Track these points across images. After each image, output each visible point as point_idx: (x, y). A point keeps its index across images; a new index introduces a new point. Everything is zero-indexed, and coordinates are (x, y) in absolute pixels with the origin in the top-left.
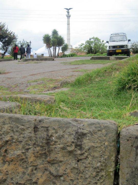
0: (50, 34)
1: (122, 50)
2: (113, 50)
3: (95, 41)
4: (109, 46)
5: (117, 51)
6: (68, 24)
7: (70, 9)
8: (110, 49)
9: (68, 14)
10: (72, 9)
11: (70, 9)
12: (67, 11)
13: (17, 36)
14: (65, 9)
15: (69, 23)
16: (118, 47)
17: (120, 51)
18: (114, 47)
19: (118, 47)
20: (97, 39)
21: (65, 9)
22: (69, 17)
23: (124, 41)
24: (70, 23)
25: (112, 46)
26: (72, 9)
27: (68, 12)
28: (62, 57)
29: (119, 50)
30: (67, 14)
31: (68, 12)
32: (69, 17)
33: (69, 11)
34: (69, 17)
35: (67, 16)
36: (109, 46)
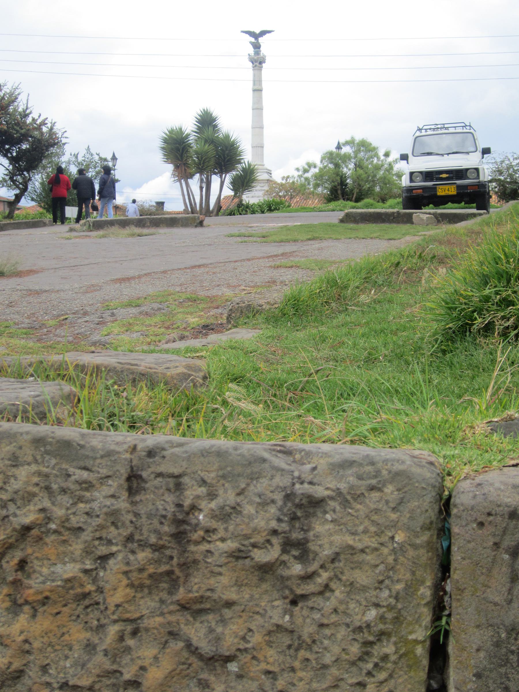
0: (189, 126)
1: (459, 187)
2: (424, 188)
3: (357, 152)
4: (412, 174)
5: (441, 192)
6: (254, 90)
7: (263, 33)
9: (257, 53)
10: (269, 32)
11: (263, 33)
12: (253, 40)
16: (444, 176)
17: (452, 191)
18: (429, 175)
20: (364, 146)
22: (258, 62)
23: (468, 153)
24: (264, 85)
25: (421, 172)
26: (269, 32)
27: (257, 46)
28: (231, 214)
29: (447, 187)
30: (251, 50)
31: (257, 46)
32: (258, 62)
33: (260, 40)
34: (261, 63)
35: (253, 61)
36: (412, 174)
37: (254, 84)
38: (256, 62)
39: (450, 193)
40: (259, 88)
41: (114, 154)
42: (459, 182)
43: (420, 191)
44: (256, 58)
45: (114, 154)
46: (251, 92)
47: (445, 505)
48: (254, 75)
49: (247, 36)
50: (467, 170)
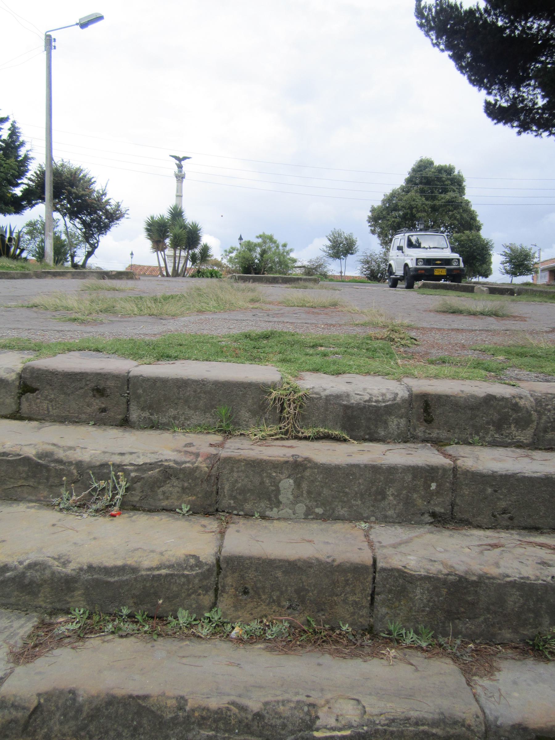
1: (448, 270)
4: (417, 259)
5: (436, 273)
6: (177, 196)
7: (185, 158)
8: (418, 267)
9: (181, 172)
10: (189, 158)
11: (185, 158)
12: (178, 162)
13: (128, 212)
14: (173, 156)
15: (181, 192)
16: (439, 262)
17: (444, 273)
18: (428, 261)
19: (439, 262)
20: (268, 239)
21: (173, 156)
22: (180, 177)
23: (443, 248)
25: (423, 259)
26: (189, 158)
27: (180, 167)
28: (193, 276)
29: (440, 270)
30: (176, 169)
31: (180, 167)
32: (180, 177)
33: (183, 163)
35: (177, 176)
36: (417, 259)
37: (177, 192)
38: (179, 177)
39: (442, 274)
40: (181, 195)
41: (241, 236)
42: (447, 267)
43: (423, 272)
44: (179, 174)
45: (241, 236)
46: (175, 197)
47: (86, 448)
48: (178, 186)
49: (174, 159)
50: (453, 259)
